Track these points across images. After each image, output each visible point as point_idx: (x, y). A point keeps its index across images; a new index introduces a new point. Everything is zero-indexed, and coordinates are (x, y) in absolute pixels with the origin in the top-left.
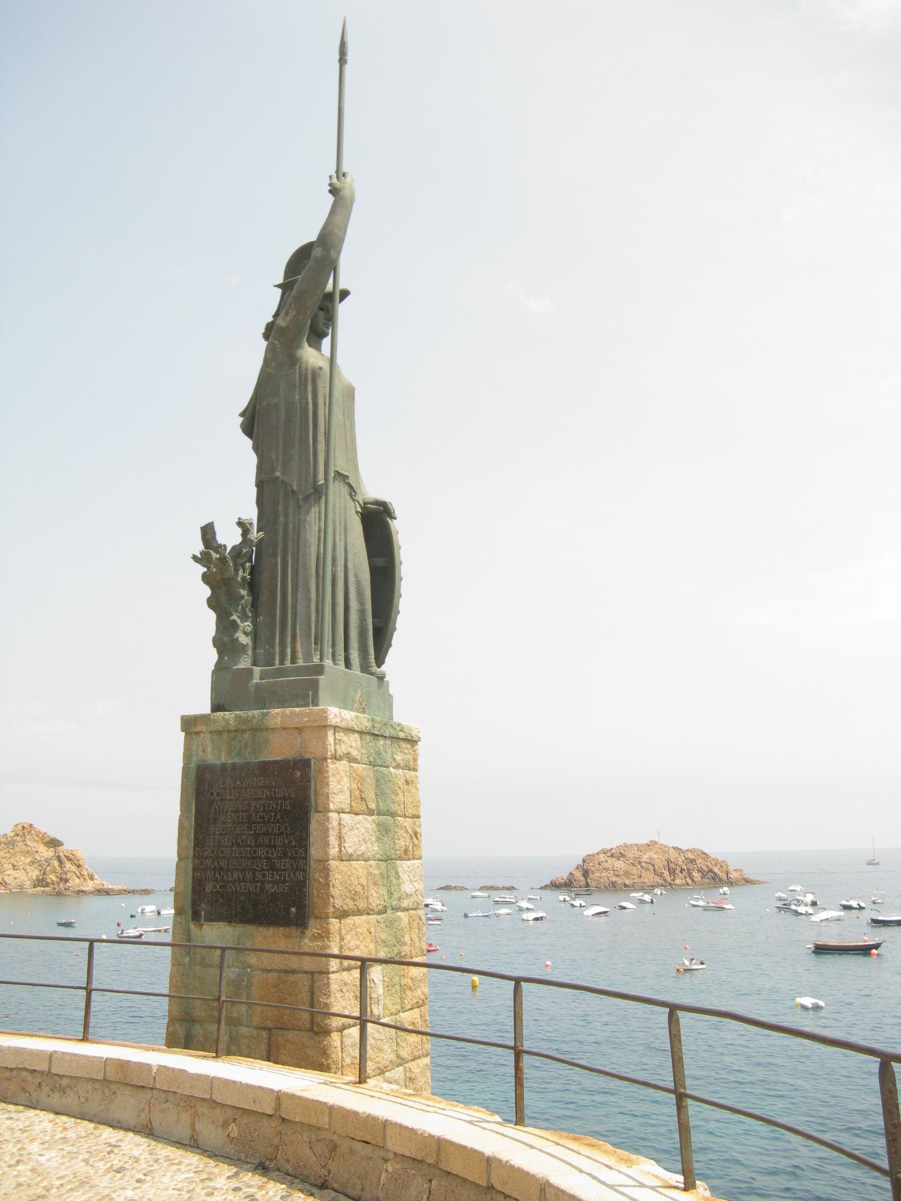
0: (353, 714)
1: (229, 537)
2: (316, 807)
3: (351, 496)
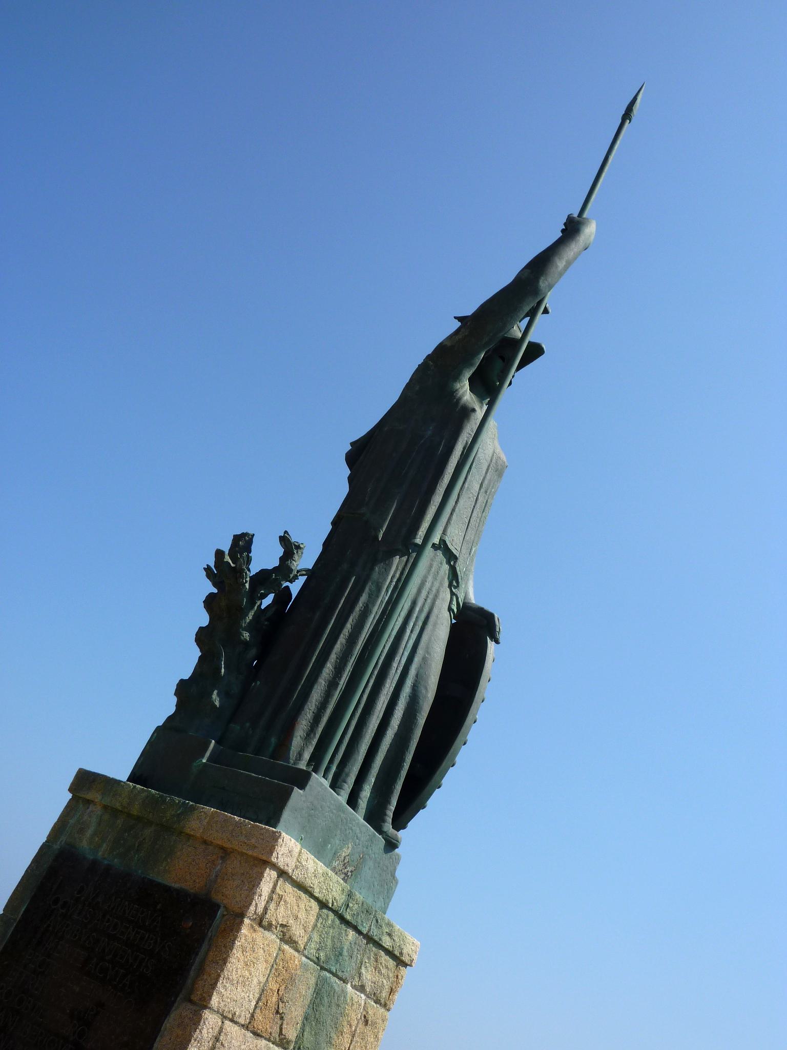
0: (321, 867)
1: (265, 556)
2: (192, 991)
3: (450, 586)
